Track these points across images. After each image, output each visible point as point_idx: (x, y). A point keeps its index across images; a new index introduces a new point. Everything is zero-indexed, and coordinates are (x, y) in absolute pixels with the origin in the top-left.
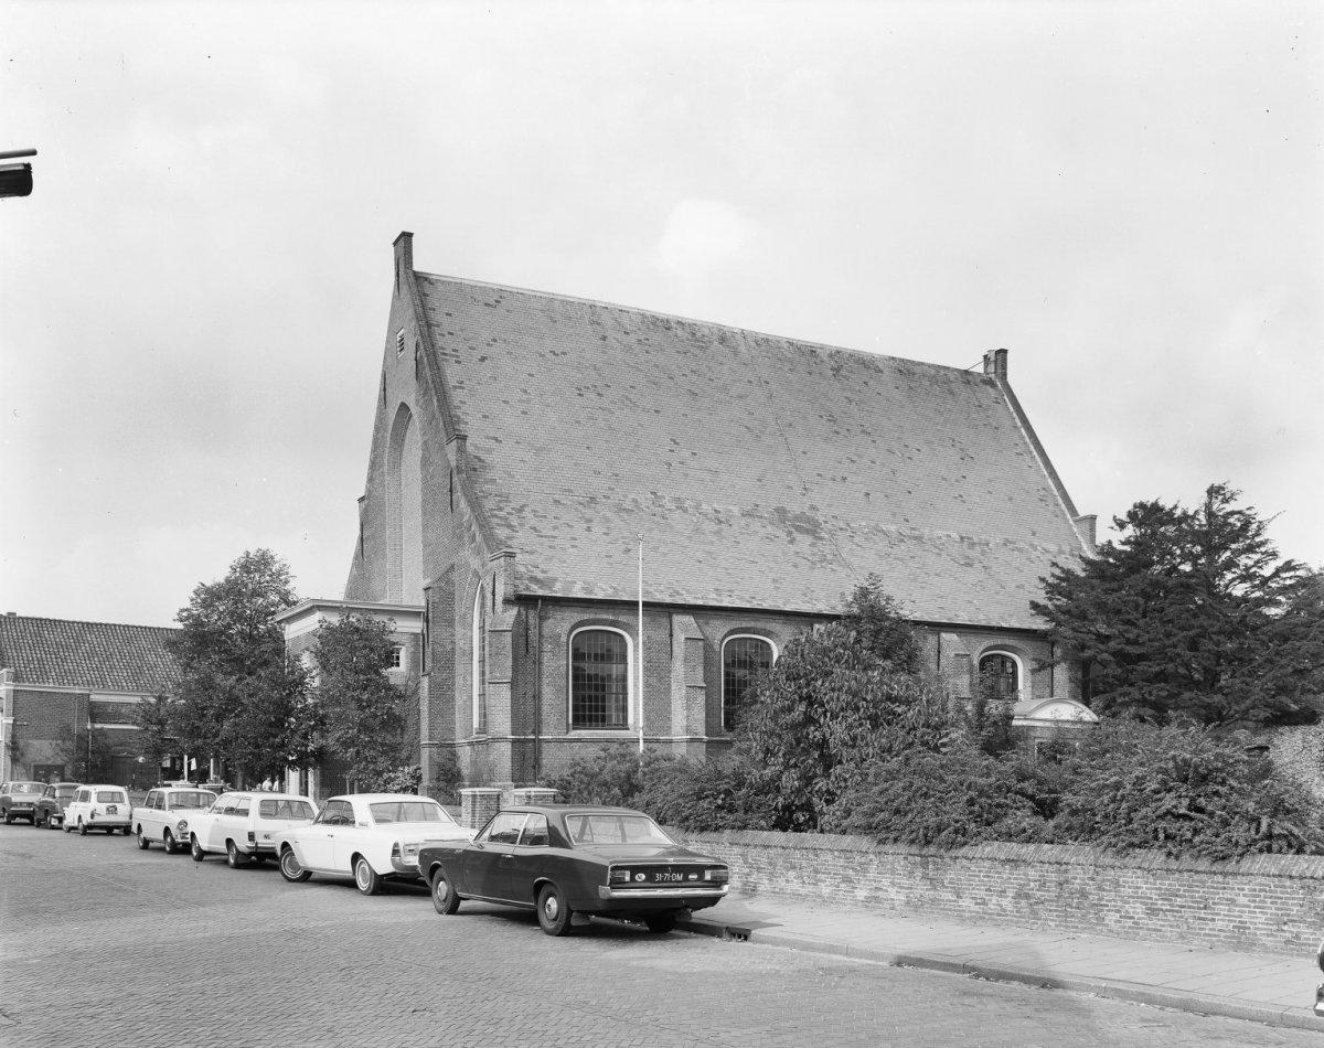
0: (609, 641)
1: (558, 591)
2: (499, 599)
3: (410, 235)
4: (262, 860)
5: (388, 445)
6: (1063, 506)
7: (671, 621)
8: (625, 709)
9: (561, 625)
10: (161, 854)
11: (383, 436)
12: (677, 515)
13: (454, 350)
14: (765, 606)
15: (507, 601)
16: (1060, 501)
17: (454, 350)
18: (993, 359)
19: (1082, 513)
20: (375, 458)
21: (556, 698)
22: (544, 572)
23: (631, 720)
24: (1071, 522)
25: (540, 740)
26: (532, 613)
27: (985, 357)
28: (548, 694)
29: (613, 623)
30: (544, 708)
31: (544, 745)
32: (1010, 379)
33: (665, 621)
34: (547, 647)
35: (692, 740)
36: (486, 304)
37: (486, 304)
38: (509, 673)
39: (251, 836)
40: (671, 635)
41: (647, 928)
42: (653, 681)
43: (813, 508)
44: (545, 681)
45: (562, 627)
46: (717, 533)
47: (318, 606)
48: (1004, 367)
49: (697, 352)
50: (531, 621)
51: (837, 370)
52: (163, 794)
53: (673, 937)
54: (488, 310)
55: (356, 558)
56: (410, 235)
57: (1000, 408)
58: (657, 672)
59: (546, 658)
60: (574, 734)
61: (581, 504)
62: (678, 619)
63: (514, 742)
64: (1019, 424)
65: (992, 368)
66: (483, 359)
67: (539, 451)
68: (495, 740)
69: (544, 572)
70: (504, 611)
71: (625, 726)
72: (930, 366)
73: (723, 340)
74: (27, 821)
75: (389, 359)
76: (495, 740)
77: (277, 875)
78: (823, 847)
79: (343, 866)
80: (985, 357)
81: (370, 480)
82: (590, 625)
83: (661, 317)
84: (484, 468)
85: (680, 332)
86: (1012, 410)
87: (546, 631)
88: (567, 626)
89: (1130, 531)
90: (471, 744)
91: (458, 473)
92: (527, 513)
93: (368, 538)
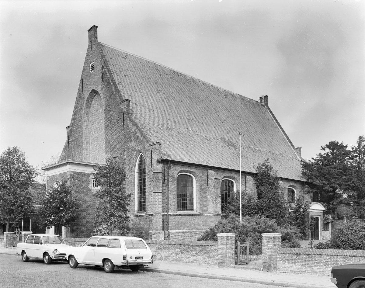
0: (188, 178)
1: (173, 158)
2: (154, 161)
3: (97, 27)
4: (61, 260)
5: (84, 106)
6: (290, 144)
7: (207, 172)
8: (192, 204)
9: (175, 171)
10: (41, 264)
11: (81, 103)
12: (196, 136)
13: (115, 71)
14: (233, 168)
15: (158, 162)
16: (289, 143)
17: (115, 71)
18: (263, 98)
19: (296, 147)
20: (77, 111)
21: (174, 200)
22: (166, 152)
23: (195, 208)
24: (293, 149)
25: (169, 215)
26: (166, 166)
27: (261, 98)
28: (170, 196)
29: (190, 172)
30: (170, 202)
31: (170, 217)
32: (269, 105)
33: (205, 172)
34: (170, 180)
35: (217, 215)
36: (122, 57)
37: (122, 57)
38: (161, 189)
39: (125, 258)
40: (207, 177)
41: (131, 270)
42: (202, 193)
43: (231, 138)
44: (170, 192)
45: (175, 172)
46: (209, 143)
47: (69, 162)
48: (267, 101)
49: (188, 84)
50: (166, 170)
51: (226, 96)
52: (40, 237)
53: (139, 273)
54: (124, 59)
55: (65, 148)
56: (97, 27)
57: (267, 113)
58: (203, 190)
59: (170, 184)
60: (179, 212)
61: (167, 130)
62: (211, 172)
63: (163, 215)
64: (273, 119)
65: (263, 101)
66: (125, 76)
67: (150, 110)
68: (156, 214)
69: (166, 152)
70: (157, 165)
71: (192, 210)
72: (248, 98)
73: (194, 81)
74: (130, 270)
75: (85, 74)
76: (156, 214)
77: (68, 265)
78: (330, 256)
79: (41, 256)
80: (261, 98)
81: (73, 119)
82: (183, 172)
83: (175, 71)
84: (134, 114)
85: (181, 77)
86: (271, 114)
87: (170, 174)
88: (177, 172)
89: (328, 150)
90: (135, 216)
91: (127, 114)
92: (152, 131)
93: (72, 141)
